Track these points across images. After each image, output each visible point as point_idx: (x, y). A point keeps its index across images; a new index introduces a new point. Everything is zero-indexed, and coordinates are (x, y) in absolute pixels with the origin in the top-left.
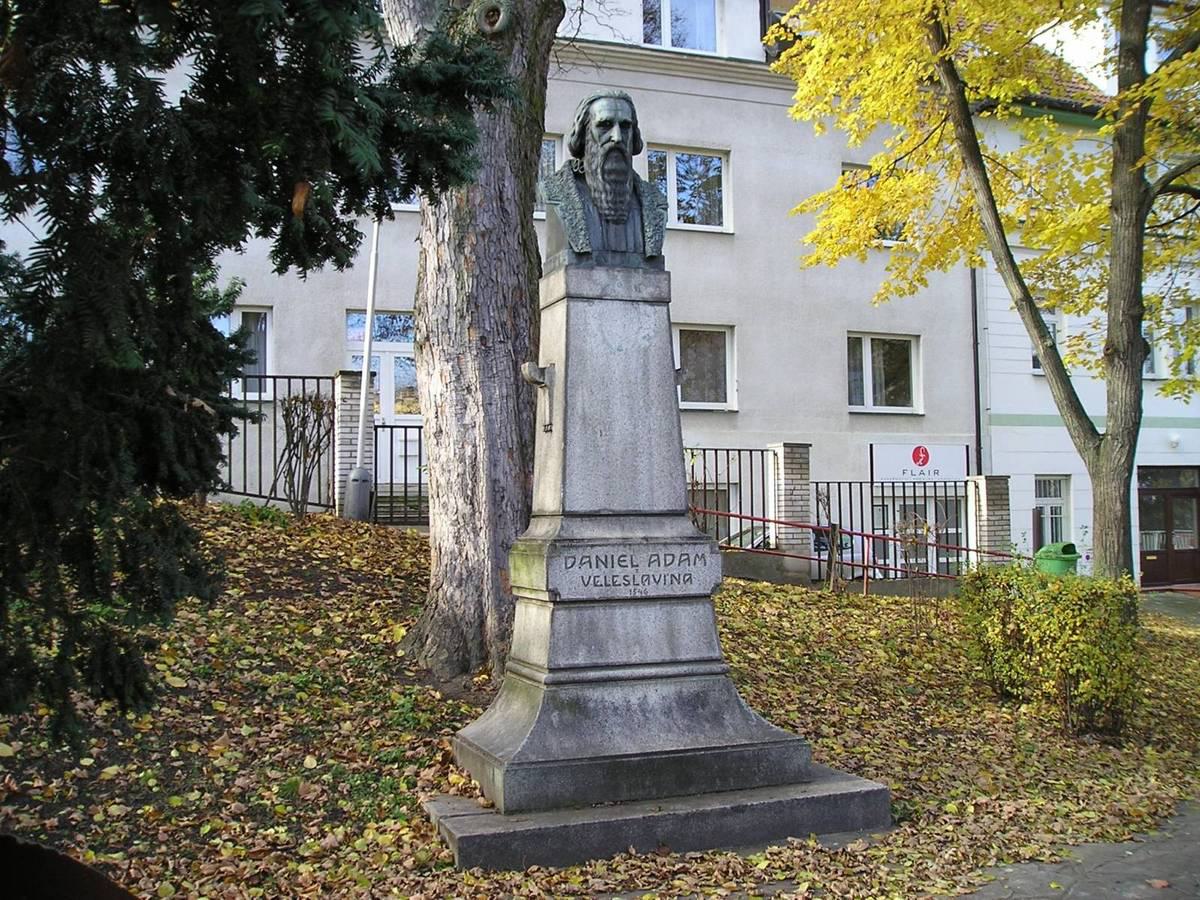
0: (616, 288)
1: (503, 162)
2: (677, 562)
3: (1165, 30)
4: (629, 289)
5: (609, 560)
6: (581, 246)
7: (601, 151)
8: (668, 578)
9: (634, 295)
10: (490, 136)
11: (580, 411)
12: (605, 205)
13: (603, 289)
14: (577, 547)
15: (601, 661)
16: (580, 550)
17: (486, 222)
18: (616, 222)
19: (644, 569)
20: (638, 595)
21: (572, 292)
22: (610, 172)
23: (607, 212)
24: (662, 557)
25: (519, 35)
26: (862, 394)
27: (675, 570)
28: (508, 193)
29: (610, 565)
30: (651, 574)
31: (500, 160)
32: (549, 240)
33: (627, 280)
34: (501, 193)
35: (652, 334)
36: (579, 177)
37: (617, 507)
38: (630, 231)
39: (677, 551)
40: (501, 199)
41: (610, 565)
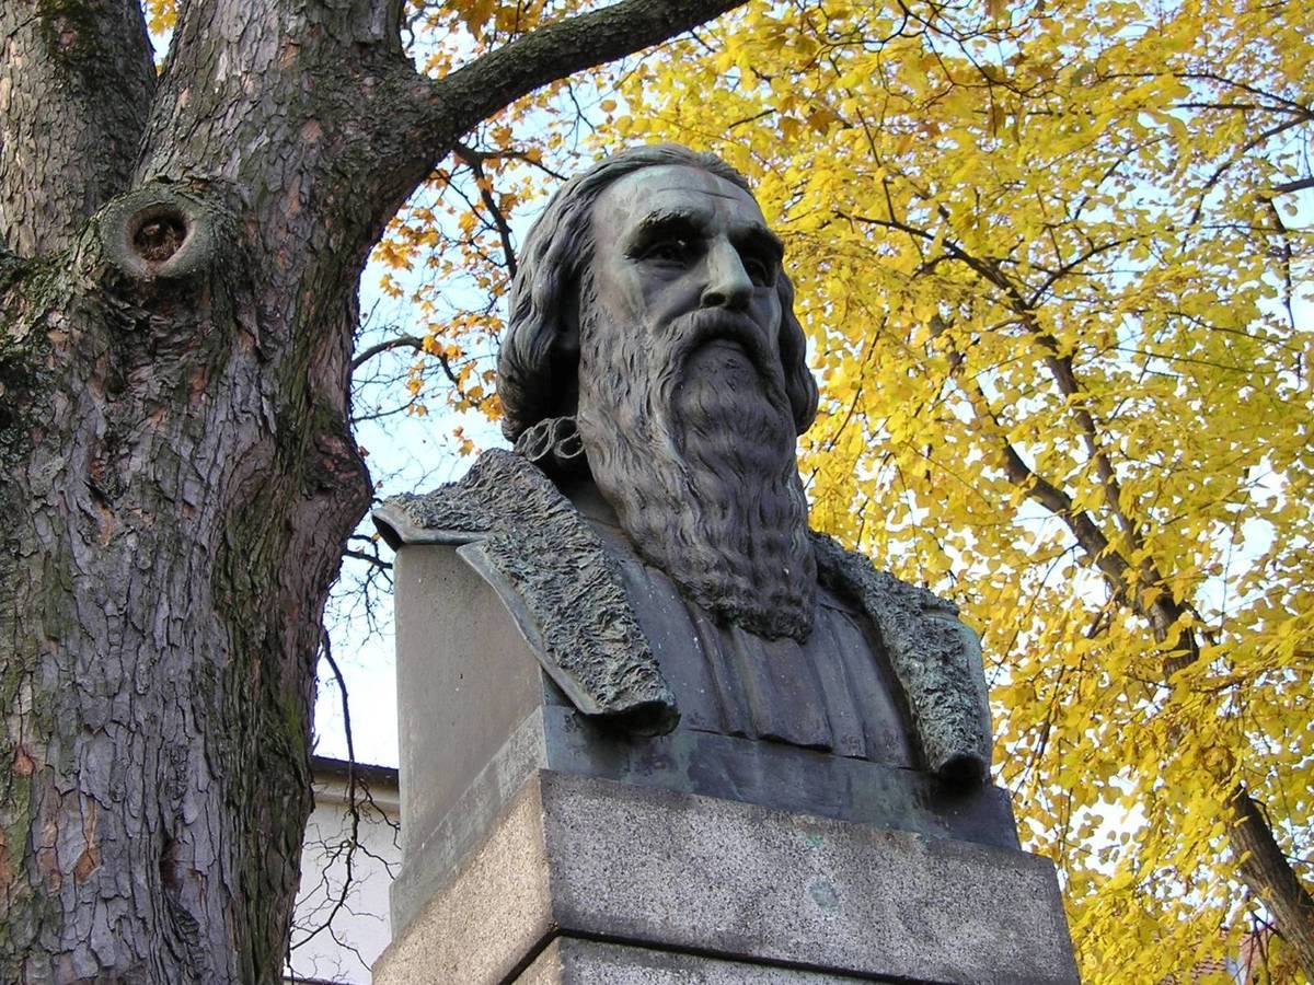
0: (811, 908)
1: (177, 724)
4: (871, 919)
6: (610, 683)
7: (660, 348)
10: (133, 627)
12: (701, 551)
13: (749, 908)
17: (102, 939)
18: (764, 628)
21: (594, 901)
22: (711, 421)
23: (715, 577)
25: (248, 320)
28: (199, 850)
31: (170, 718)
32: (558, 246)
34: (168, 843)
36: (571, 476)
38: (828, 671)
40: (167, 868)
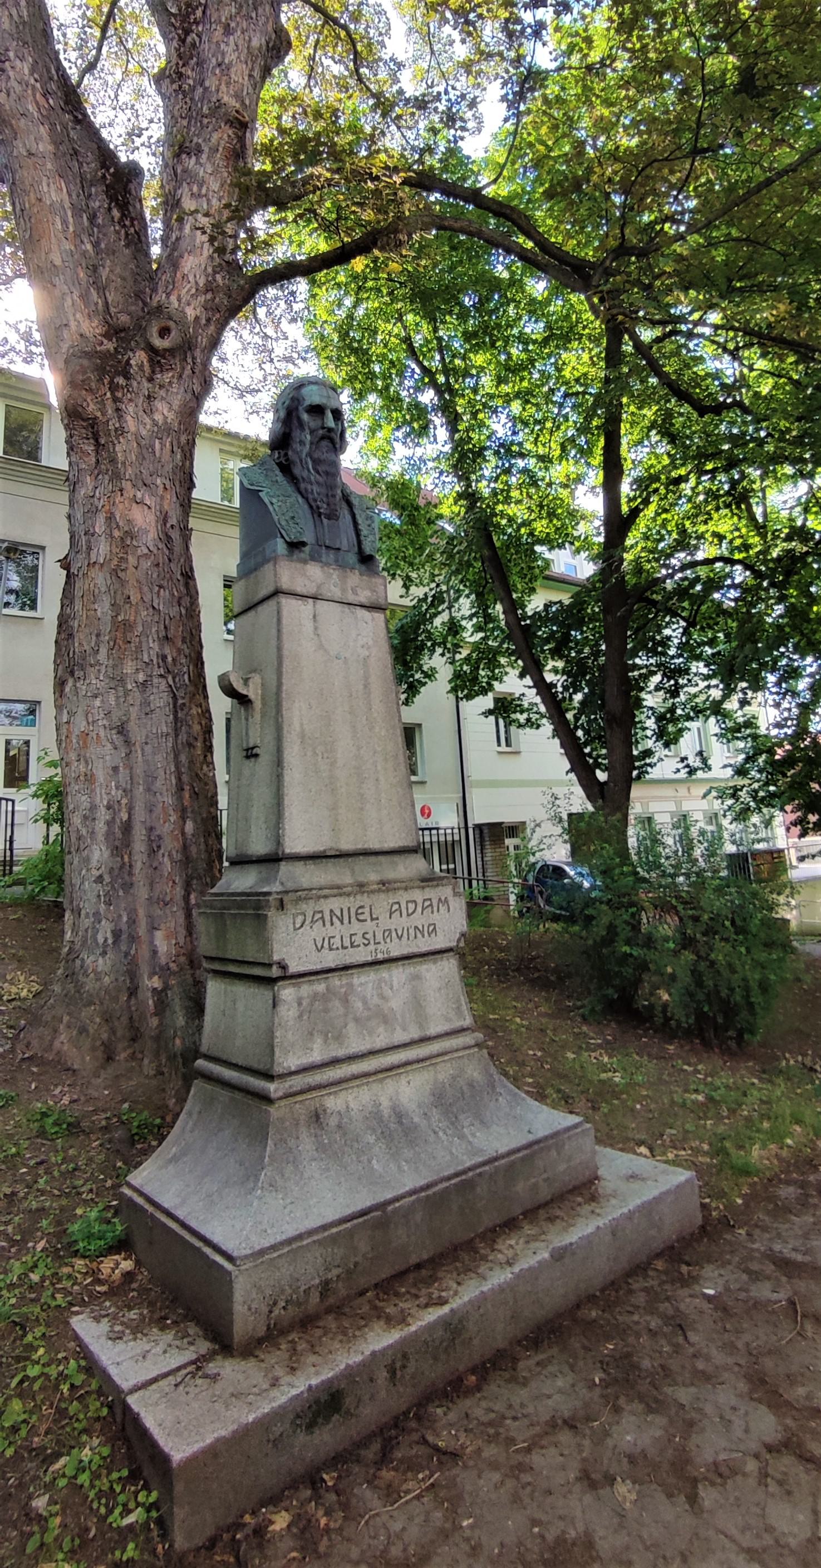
2: (419, 909)
3: (414, 171)
4: (344, 590)
5: (345, 913)
8: (412, 931)
9: (351, 598)
11: (298, 729)
13: (319, 587)
14: (307, 899)
15: (341, 1053)
16: (311, 902)
19: (385, 922)
20: (380, 956)
24: (403, 906)
26: (205, 687)
27: (419, 920)
29: (346, 921)
30: (393, 928)
33: (343, 579)
35: (371, 643)
37: (346, 845)
39: (418, 895)
41: (346, 921)
